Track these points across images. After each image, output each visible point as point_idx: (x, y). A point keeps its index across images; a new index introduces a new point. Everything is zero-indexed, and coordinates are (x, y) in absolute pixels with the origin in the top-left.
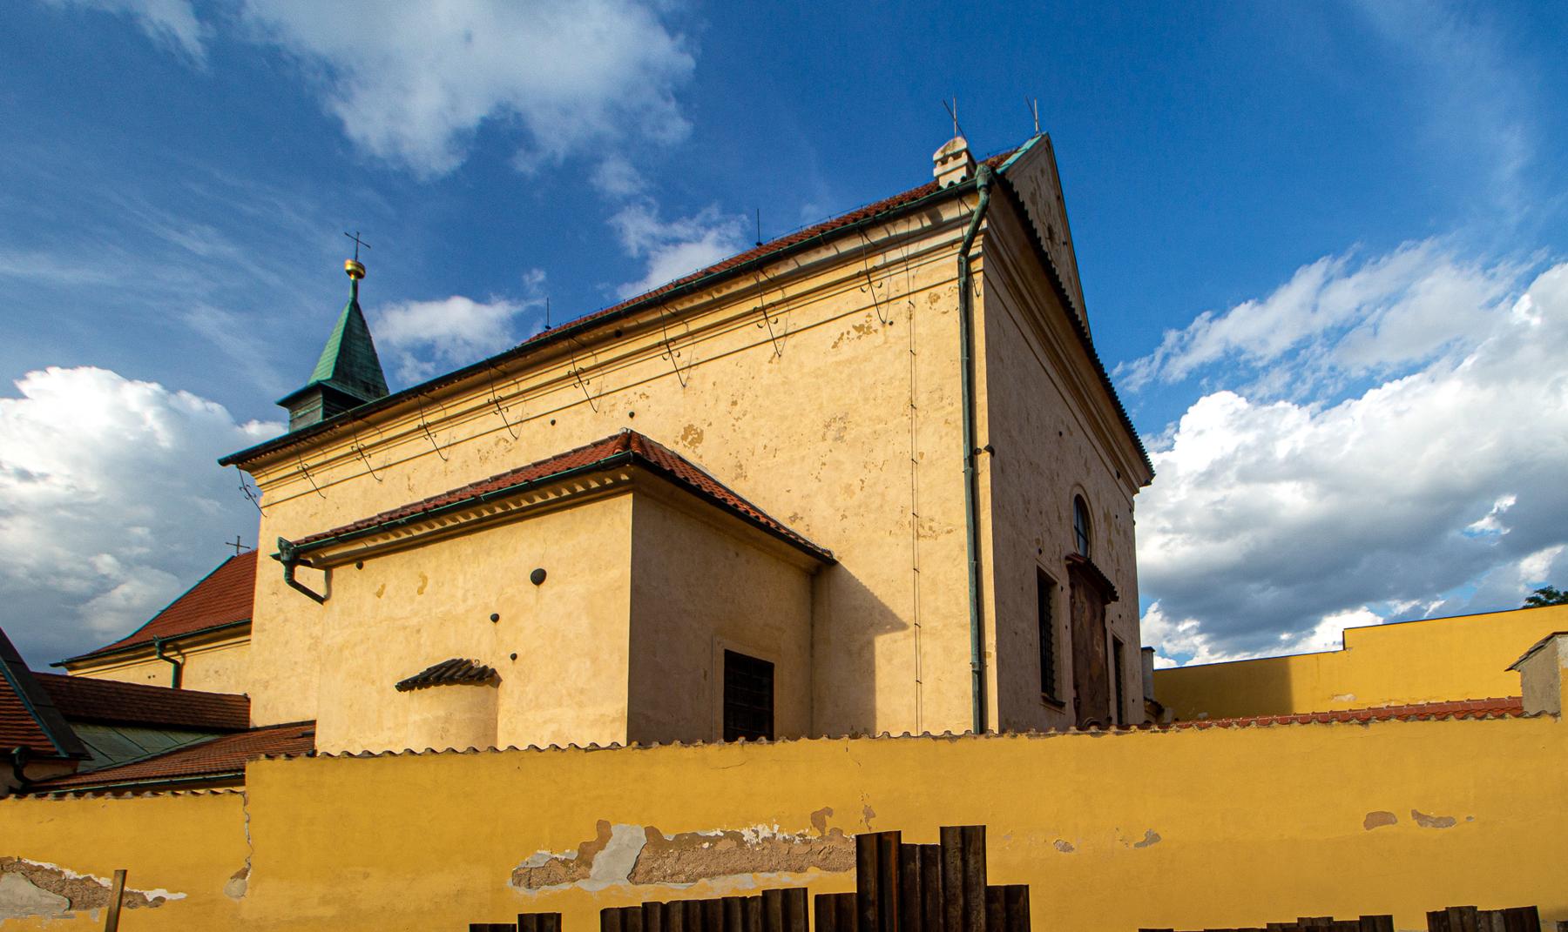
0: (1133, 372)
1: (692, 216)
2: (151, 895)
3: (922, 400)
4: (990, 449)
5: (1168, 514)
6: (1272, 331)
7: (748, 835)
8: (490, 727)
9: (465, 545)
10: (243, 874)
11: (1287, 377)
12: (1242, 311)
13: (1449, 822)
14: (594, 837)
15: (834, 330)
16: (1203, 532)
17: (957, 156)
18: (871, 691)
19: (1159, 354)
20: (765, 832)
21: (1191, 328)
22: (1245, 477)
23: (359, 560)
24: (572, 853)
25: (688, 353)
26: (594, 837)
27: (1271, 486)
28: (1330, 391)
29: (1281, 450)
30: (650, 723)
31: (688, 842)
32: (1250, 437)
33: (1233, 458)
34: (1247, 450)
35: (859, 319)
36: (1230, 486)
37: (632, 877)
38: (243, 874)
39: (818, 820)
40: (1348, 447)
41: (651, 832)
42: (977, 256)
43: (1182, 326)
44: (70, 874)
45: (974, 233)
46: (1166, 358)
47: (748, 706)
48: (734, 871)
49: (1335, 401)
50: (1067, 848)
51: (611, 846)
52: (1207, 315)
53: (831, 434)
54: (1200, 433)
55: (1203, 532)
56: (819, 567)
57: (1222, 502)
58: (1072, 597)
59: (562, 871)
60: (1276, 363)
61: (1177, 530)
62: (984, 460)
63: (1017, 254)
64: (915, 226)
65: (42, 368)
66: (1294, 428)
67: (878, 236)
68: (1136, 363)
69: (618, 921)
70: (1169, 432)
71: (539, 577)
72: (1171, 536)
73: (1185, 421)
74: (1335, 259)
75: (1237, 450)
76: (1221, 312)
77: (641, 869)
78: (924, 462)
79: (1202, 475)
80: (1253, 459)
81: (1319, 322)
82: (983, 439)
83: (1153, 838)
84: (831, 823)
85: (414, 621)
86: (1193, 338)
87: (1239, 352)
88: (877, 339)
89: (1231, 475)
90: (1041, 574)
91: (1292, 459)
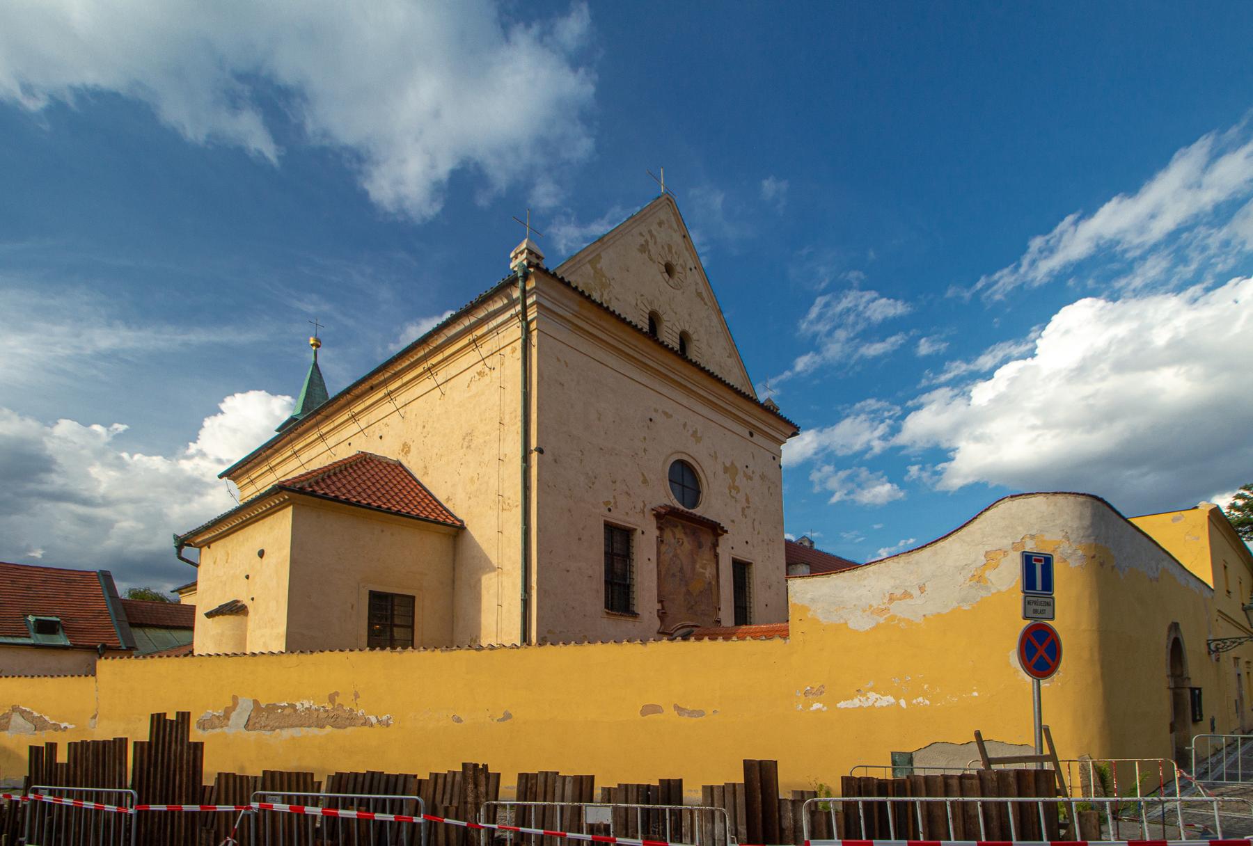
0: (996, 282)
1: (602, 217)
2: (63, 725)
3: (506, 421)
4: (540, 451)
5: (1036, 412)
6: (1152, 216)
7: (299, 706)
8: (242, 640)
9: (240, 535)
10: (95, 717)
11: (1164, 264)
12: (1107, 209)
13: (701, 713)
14: (230, 704)
15: (467, 376)
16: (1072, 425)
17: (522, 253)
18: (479, 611)
19: (1026, 261)
20: (307, 705)
21: (1057, 231)
22: (1120, 367)
23: (208, 543)
24: (220, 712)
25: (402, 399)
26: (230, 704)
27: (1149, 374)
28: (1220, 268)
29: (1161, 338)
30: (303, 638)
31: (272, 708)
32: (1121, 330)
33: (1105, 352)
34: (1122, 342)
35: (479, 367)
36: (1103, 379)
37: (247, 726)
38: (95, 717)
39: (332, 698)
40: (1237, 328)
41: (256, 702)
42: (532, 321)
43: (1047, 229)
44: (36, 714)
45: (525, 308)
46: (1033, 263)
47: (389, 622)
48: (292, 726)
49: (1221, 281)
50: (459, 720)
51: (238, 709)
52: (1070, 219)
53: (466, 444)
54: (1067, 332)
55: (1072, 425)
56: (456, 530)
57: (1093, 395)
58: (661, 541)
59: (217, 721)
60: (1154, 249)
61: (1047, 426)
62: (534, 457)
63: (576, 308)
64: (499, 304)
65: (232, 394)
66: (1168, 318)
67: (481, 314)
68: (997, 275)
69: (942, 784)
70: (1032, 335)
71: (261, 554)
72: (1040, 432)
73: (1056, 319)
74: (1224, 130)
75: (1110, 344)
76: (1089, 211)
77: (251, 723)
78: (506, 460)
79: (1072, 370)
80: (1128, 350)
81: (1208, 197)
82: (534, 444)
83: (508, 716)
84: (338, 700)
85: (224, 578)
86: (1059, 241)
87: (1114, 243)
88: (487, 380)
89: (1105, 367)
90: (610, 528)
91: (1174, 344)
